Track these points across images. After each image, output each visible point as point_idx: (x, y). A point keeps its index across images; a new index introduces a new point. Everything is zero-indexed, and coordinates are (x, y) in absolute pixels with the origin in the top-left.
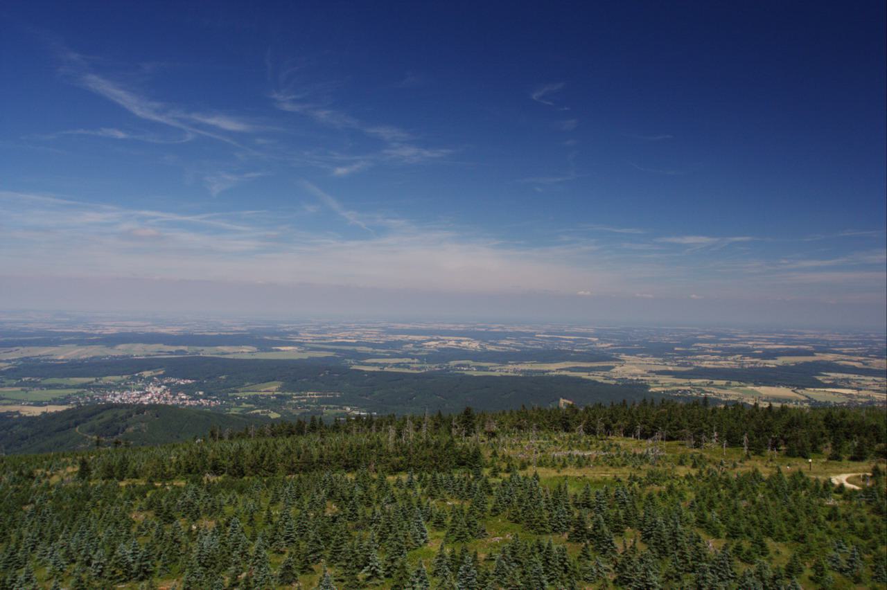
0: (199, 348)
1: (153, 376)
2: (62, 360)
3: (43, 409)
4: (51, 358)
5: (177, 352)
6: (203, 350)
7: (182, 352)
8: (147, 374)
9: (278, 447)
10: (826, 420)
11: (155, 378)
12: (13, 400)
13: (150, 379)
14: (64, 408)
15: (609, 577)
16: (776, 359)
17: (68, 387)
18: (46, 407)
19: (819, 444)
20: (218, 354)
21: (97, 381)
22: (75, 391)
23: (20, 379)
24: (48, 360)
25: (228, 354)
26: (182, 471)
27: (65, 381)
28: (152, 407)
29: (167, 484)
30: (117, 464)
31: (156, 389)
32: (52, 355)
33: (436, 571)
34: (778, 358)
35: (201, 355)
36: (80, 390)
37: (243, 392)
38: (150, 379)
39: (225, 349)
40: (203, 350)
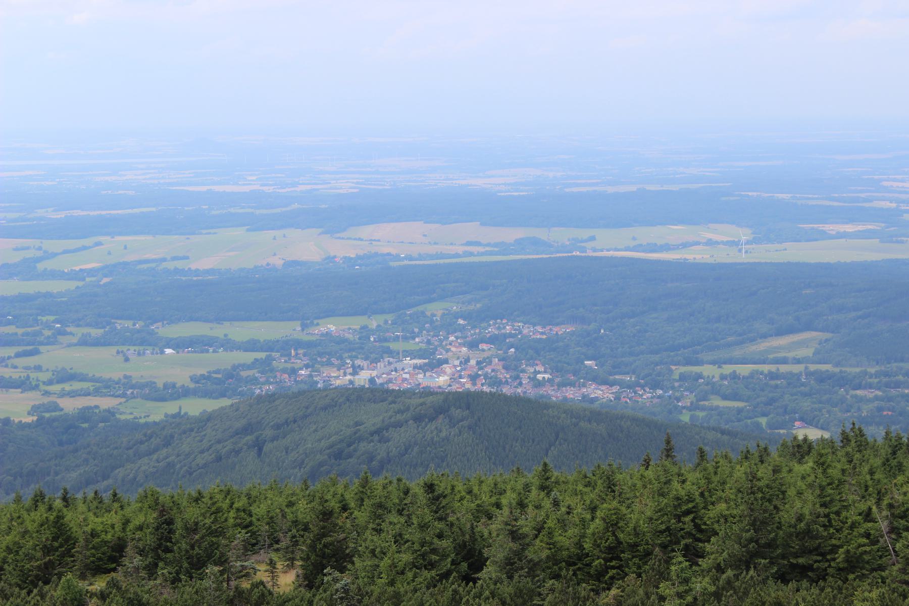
0: (585, 233)
2: (859, 225)
3: (171, 408)
6: (593, 238)
7: (535, 242)
8: (436, 309)
9: (709, 477)
12: (93, 380)
13: (449, 325)
14: (225, 402)
15: (165, 571)
16: (222, 324)
17: (229, 345)
22: (249, 357)
25: (667, 248)
27: (218, 331)
28: (466, 400)
33: (273, 595)
34: (224, 322)
36: (262, 355)
37: (713, 363)
38: (449, 325)
39: (675, 232)
40: (593, 238)
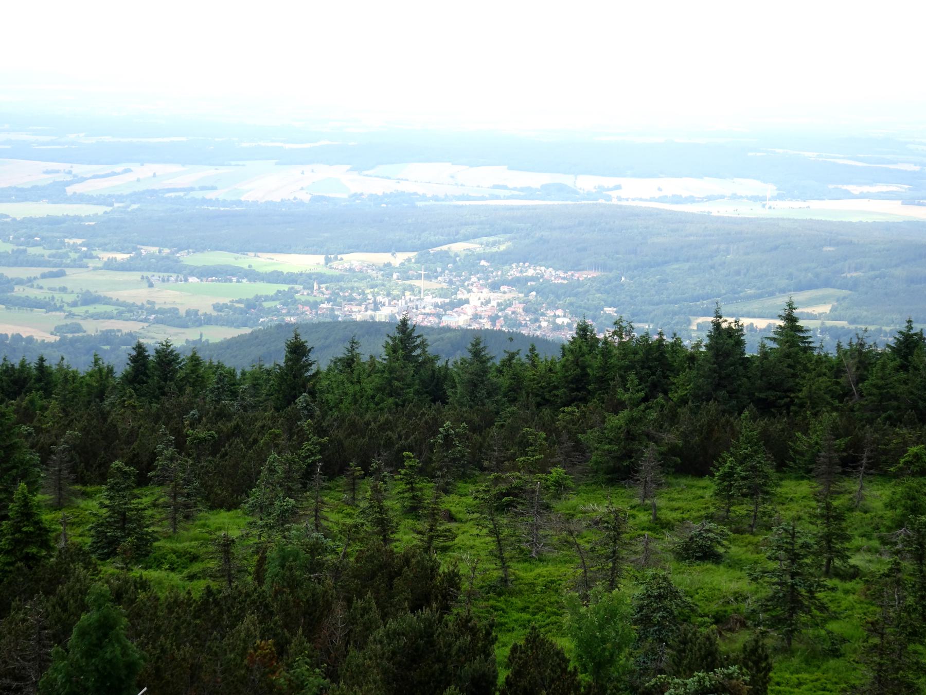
1: (480, 257)
4: (210, 195)
5: (546, 191)
6: (618, 187)
10: (214, 308)
11: (483, 263)
18: (199, 330)
19: (384, 499)
20: (662, 200)
21: (160, 251)
22: (271, 289)
23: (135, 249)
24: (204, 201)
25: (691, 200)
26: (872, 526)
29: (816, 547)
30: (433, 484)
31: (486, 293)
32: (213, 188)
35: (615, 202)
36: (285, 287)
40: (618, 187)
